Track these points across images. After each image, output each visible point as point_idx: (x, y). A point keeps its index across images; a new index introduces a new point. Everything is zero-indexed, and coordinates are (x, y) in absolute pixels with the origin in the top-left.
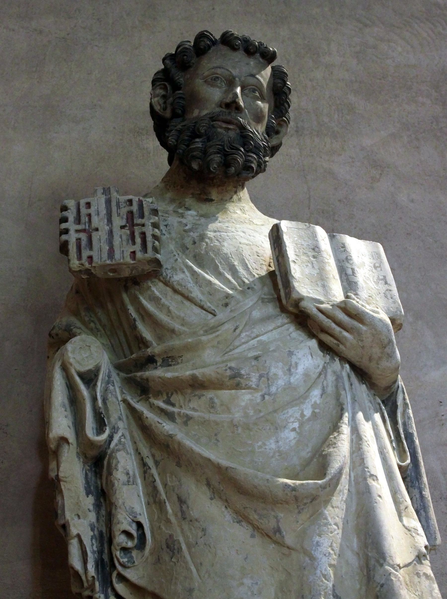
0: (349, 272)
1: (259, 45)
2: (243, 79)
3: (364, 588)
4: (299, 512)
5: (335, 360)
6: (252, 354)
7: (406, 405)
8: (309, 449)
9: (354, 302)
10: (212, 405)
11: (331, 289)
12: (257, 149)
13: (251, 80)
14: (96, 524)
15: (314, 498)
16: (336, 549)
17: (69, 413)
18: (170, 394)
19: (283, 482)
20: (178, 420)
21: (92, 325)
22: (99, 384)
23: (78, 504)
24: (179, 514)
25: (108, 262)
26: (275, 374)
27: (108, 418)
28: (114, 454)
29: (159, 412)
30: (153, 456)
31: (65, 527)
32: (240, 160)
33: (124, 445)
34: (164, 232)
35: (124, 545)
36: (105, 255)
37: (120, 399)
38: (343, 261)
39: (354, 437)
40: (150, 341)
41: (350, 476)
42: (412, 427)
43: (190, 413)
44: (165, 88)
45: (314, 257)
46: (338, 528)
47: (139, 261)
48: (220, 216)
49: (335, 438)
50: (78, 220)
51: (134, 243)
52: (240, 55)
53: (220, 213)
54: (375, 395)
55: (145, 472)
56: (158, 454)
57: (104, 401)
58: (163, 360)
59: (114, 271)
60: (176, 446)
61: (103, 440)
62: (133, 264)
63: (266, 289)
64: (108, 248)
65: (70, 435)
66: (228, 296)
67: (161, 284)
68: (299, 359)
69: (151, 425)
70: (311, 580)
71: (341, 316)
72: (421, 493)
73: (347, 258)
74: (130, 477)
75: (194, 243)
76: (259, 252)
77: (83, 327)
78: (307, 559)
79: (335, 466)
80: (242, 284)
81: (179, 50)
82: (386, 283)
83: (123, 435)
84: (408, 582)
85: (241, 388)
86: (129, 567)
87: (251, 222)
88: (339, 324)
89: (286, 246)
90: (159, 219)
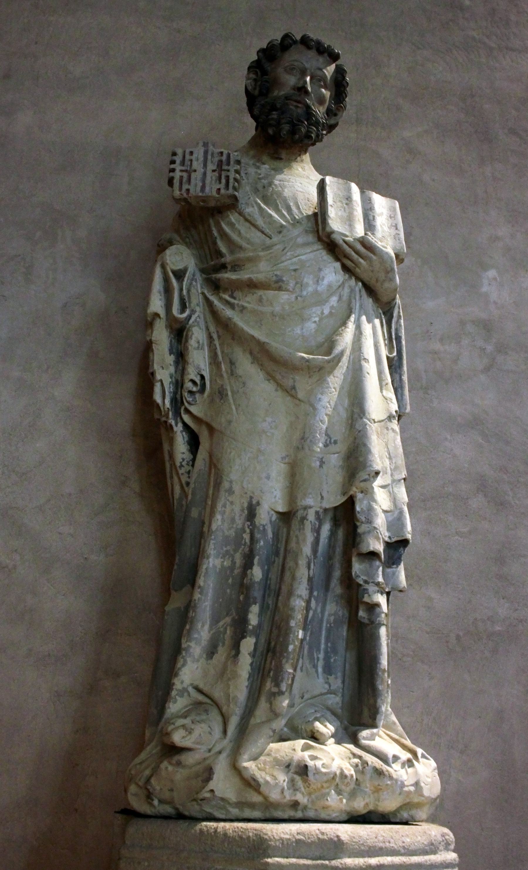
0: (371, 218)
1: (327, 47)
2: (313, 71)
3: (347, 432)
4: (310, 377)
5: (351, 278)
6: (292, 268)
7: (399, 317)
8: (324, 336)
9: (370, 238)
10: (260, 300)
11: (355, 228)
12: (317, 124)
13: (319, 73)
14: (174, 375)
15: (321, 369)
16: (332, 404)
17: (163, 297)
18: (234, 290)
19: (301, 356)
20: (237, 308)
21: (187, 240)
22: (186, 279)
23: (163, 360)
24: (229, 372)
25: (200, 194)
26: (307, 283)
27: (190, 303)
28: (191, 329)
29: (225, 302)
30: (218, 332)
31: (153, 374)
32: (303, 130)
33: (198, 323)
34: (244, 178)
35: (190, 389)
36: (199, 189)
37: (200, 291)
38: (368, 210)
39: (357, 332)
40: (225, 254)
41: (350, 357)
42: (401, 332)
43: (246, 304)
44: (256, 74)
45: (347, 204)
46: (336, 391)
47: (222, 195)
48: (286, 171)
49: (342, 330)
50: (183, 163)
51: (220, 183)
52: (312, 53)
53: (287, 168)
54: (378, 307)
55: (211, 343)
56: (221, 331)
57: (189, 291)
58: (232, 267)
59: (203, 201)
60: (232, 326)
61: (183, 318)
62: (218, 197)
63: (310, 225)
64: (201, 184)
65: (162, 312)
66: (282, 226)
67: (236, 214)
68: (326, 274)
69: (218, 311)
70: (311, 422)
71: (359, 247)
72: (400, 377)
73: (371, 208)
74: (199, 345)
75: (264, 187)
76: (309, 198)
77: (181, 241)
78: (311, 408)
79: (338, 349)
80: (294, 219)
81: (269, 45)
82: (397, 229)
83: (198, 316)
84: (379, 433)
85: (282, 291)
86: (192, 404)
87: (308, 177)
88: (357, 252)
89: (327, 194)
90: (241, 168)
